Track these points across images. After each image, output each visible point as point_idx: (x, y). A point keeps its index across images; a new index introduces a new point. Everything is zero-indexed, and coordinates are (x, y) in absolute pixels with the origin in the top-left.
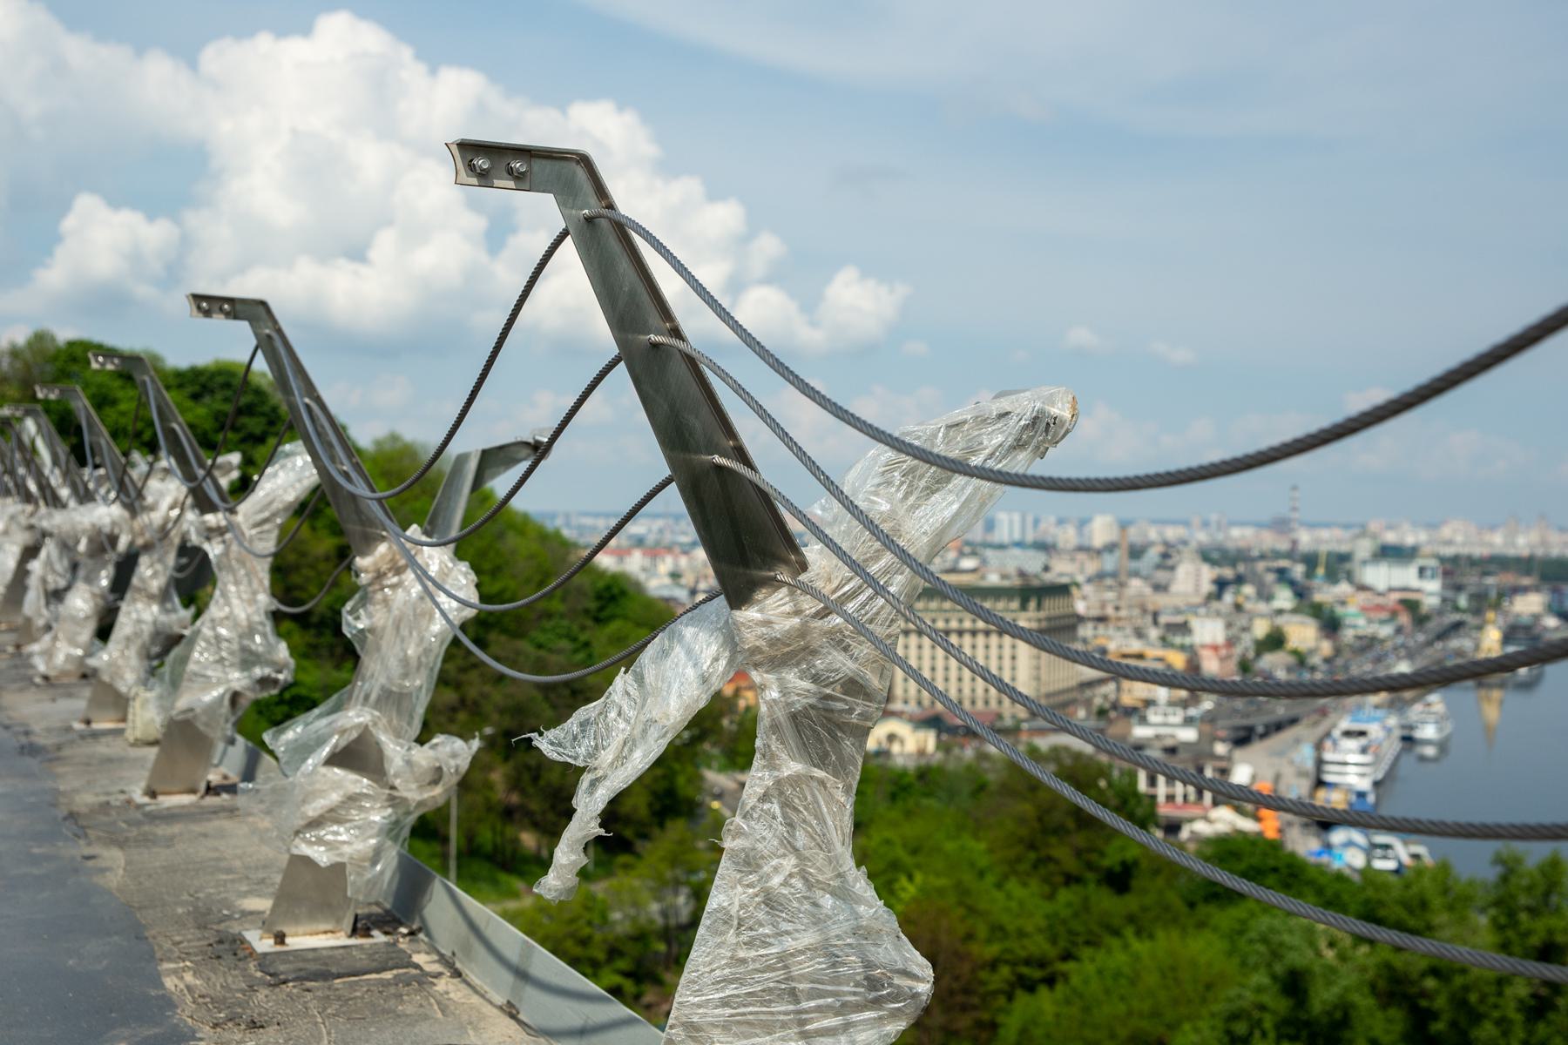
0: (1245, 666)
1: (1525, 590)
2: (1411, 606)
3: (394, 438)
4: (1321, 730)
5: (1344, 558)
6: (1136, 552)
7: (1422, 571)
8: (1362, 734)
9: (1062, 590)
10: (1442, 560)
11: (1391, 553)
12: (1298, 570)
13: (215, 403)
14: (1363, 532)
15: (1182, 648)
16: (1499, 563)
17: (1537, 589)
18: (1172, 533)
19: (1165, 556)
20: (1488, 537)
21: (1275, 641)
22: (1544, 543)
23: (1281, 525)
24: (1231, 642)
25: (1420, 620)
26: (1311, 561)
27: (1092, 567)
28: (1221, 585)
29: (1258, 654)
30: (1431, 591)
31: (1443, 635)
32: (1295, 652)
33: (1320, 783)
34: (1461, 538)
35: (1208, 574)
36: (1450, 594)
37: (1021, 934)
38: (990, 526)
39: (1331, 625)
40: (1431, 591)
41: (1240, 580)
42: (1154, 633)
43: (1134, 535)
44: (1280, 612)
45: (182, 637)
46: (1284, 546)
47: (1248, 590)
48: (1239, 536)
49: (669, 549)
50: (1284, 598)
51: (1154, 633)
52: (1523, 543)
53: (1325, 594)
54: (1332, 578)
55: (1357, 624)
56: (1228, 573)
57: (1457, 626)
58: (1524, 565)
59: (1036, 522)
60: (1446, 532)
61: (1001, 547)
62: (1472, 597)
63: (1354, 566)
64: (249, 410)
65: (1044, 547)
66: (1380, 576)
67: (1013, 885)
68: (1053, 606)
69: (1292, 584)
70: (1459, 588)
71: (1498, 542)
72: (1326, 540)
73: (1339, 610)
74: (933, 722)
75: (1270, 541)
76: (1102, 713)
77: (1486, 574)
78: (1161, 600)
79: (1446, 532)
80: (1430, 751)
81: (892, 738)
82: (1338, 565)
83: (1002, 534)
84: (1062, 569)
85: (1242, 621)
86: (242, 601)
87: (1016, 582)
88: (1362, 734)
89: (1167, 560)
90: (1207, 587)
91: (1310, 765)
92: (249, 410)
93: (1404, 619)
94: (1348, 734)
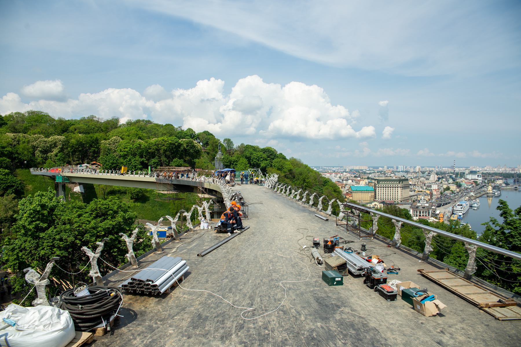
0: (441, 193)
1: (500, 179)
2: (476, 182)
3: (293, 158)
4: (454, 205)
5: (464, 173)
6: (423, 173)
7: (478, 176)
8: (461, 205)
9: (407, 180)
10: (483, 173)
11: (472, 172)
12: (454, 176)
13: (267, 154)
14: (467, 168)
15: (429, 190)
16: (496, 174)
17: (502, 179)
18: (431, 169)
19: (429, 173)
20: (494, 169)
21: (448, 189)
22: (506, 170)
23: (453, 167)
24: (438, 189)
25: (477, 185)
26: (457, 174)
27: (415, 175)
28: (439, 178)
29: (444, 191)
30: (480, 179)
31: (481, 188)
32: (451, 191)
33: (453, 214)
34: (488, 169)
35: (436, 176)
36: (484, 180)
37: (386, 233)
38: (397, 168)
39: (459, 186)
40: (480, 179)
41: (443, 178)
42: (424, 187)
43: (424, 170)
44: (449, 183)
45: (7, 124)
46: (453, 171)
47: (444, 179)
48: (444, 169)
49: (339, 173)
50: (451, 181)
51: (424, 187)
52: (501, 170)
53: (459, 180)
54: (461, 177)
55: (464, 185)
56: (441, 176)
57: (483, 186)
58: (500, 174)
59: (406, 167)
60: (486, 168)
61: (399, 172)
62: (488, 180)
63: (465, 174)
64: (271, 155)
65: (407, 172)
66: (470, 177)
67: (386, 226)
68: (405, 183)
69: (452, 178)
70: (486, 179)
71: (496, 170)
72: (462, 170)
73: (461, 183)
74: (383, 202)
75: (450, 170)
76: (414, 201)
77: (493, 176)
78: (426, 182)
79: (486, 168)
80: (475, 208)
81: (375, 205)
82: (462, 175)
83: (400, 170)
84: (408, 176)
85: (441, 185)
86: (288, 191)
87: (398, 179)
88: (461, 205)
89: (429, 174)
90: (436, 179)
91: (451, 210)
92: (271, 155)
93: (474, 185)
94: (459, 205)
